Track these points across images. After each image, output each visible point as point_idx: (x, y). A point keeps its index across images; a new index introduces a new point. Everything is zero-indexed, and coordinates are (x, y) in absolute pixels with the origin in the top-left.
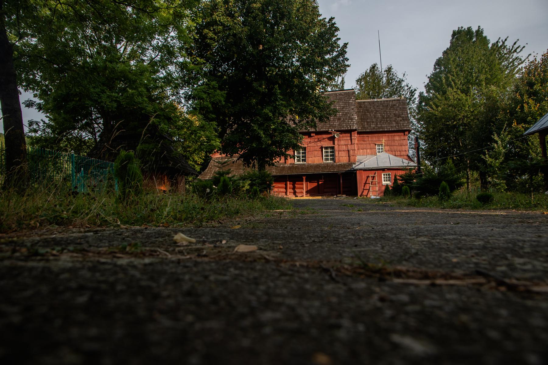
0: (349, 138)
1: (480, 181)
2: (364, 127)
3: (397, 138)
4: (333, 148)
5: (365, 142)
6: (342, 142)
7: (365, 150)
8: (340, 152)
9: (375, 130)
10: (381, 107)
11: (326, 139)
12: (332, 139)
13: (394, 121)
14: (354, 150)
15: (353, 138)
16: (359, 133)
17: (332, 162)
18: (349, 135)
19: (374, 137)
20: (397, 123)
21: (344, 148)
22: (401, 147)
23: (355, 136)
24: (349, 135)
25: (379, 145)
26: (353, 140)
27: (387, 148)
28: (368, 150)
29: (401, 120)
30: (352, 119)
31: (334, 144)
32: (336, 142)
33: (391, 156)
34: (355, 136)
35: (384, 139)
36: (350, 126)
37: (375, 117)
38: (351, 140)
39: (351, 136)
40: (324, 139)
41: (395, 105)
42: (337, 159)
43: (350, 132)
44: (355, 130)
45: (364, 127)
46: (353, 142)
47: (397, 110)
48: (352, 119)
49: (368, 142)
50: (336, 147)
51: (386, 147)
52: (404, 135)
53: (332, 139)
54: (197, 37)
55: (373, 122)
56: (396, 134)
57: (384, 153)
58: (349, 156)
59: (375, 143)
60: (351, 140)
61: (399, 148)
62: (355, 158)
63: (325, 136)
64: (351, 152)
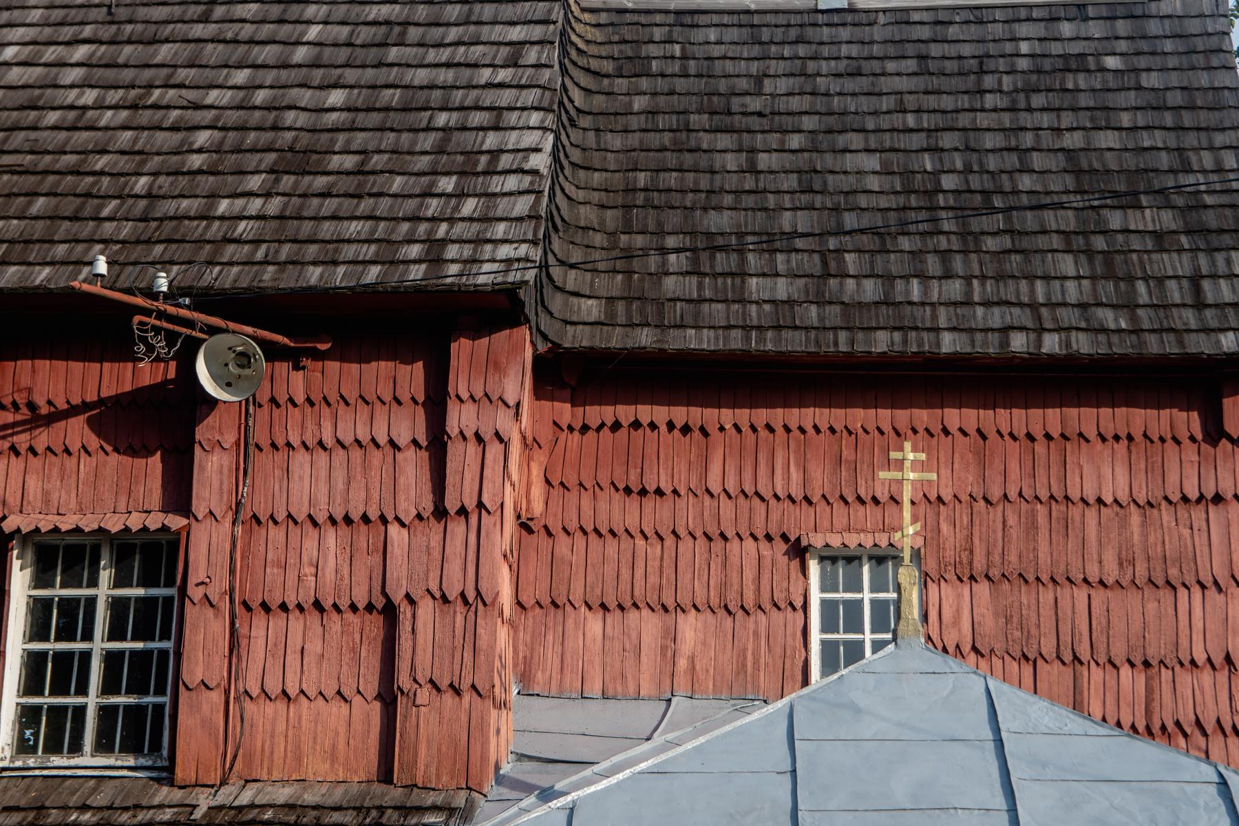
0: (408, 425)
1: (328, 363)
2: (641, 301)
3: (1105, 474)
4: (155, 556)
5: (657, 514)
6: (308, 483)
7: (649, 626)
8: (260, 632)
9: (795, 343)
10: (900, 78)
11: (77, 430)
12: (161, 425)
13: (1071, 242)
14: (476, 601)
15: (460, 418)
16: (560, 374)
17: (120, 762)
18: (412, 377)
19: (790, 450)
20: (1110, 267)
21: (329, 562)
22: (1156, 605)
23: (497, 385)
24: (412, 377)
25: (841, 560)
26: (461, 458)
27: (963, 606)
28: (690, 628)
29: (1161, 239)
30: (474, 168)
31: (178, 494)
32: (212, 472)
33: (1031, 715)
34: (497, 385)
35: (911, 465)
36: (435, 247)
37: (809, 182)
38: (437, 446)
39: (436, 403)
40: (38, 419)
41: (1075, 64)
42: (197, 723)
43: (419, 326)
44: (497, 310)
45: (641, 301)
46: (460, 491)
47: (1102, 117)
48: (474, 168)
49: (689, 513)
50: (208, 548)
51: (950, 596)
52: (1215, 432)
53: (161, 425)
54: (883, 474)
55: (772, 242)
56: (1086, 418)
57: (914, 653)
58: (388, 697)
59: (798, 522)
60: (437, 446)
61: (1133, 617)
62: (476, 731)
63: (55, 380)
64: (425, 631)
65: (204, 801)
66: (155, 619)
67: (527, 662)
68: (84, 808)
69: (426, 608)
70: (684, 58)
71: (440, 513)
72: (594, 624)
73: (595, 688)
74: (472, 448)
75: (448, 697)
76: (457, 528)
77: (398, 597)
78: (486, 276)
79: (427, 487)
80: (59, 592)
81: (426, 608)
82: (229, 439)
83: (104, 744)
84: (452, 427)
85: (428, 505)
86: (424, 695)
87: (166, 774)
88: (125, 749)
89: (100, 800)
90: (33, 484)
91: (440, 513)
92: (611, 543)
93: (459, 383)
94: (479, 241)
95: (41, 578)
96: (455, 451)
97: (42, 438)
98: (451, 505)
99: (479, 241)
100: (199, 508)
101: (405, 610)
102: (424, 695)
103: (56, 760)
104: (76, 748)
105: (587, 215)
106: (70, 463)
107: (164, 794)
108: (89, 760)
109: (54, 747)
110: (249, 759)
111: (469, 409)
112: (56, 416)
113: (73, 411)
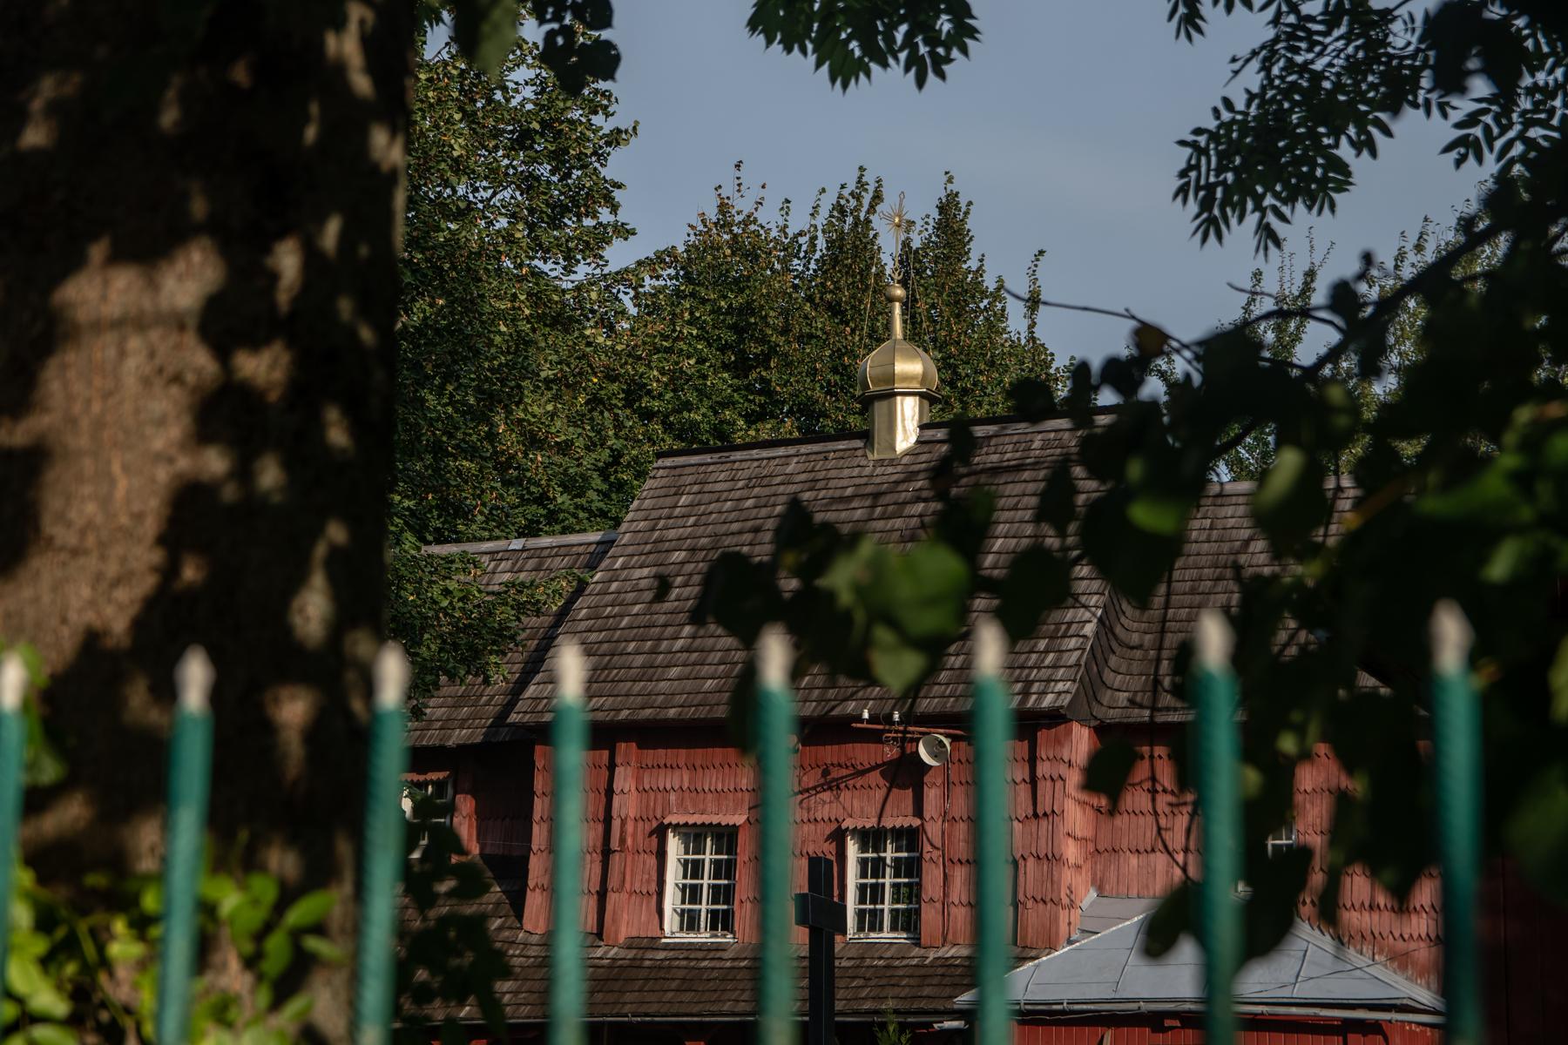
4: (909, 838)
11: (875, 777)
15: (1043, 769)
17: (901, 937)
26: (1044, 788)
31: (918, 811)
32: (932, 796)
46: (1044, 805)
62: (1054, 920)
65: (932, 955)
66: (910, 868)
67: (1102, 880)
68: (881, 958)
69: (1031, 862)
70: (1211, 528)
71: (1036, 815)
72: (1134, 860)
73: (1134, 893)
74: (1049, 783)
75: (1041, 905)
76: (1044, 823)
77: (1018, 856)
78: (1048, 701)
79: (1030, 803)
80: (870, 855)
81: (1031, 862)
82: (939, 781)
83: (894, 928)
84: (1039, 774)
85: (1030, 812)
86: (1030, 904)
87: (917, 942)
88: (903, 929)
89: (888, 954)
90: (856, 803)
91: (1036, 815)
92: (1141, 819)
93: (1042, 752)
94: (1049, 681)
95: (863, 849)
96: (1040, 785)
97: (859, 782)
98: (1040, 812)
99: (1049, 681)
100: (927, 816)
101: (1021, 862)
102: (1030, 904)
103: (873, 935)
104: (881, 930)
105: (1135, 638)
106: (871, 793)
107: (916, 951)
108: (886, 935)
109: (872, 929)
110: (954, 934)
111: (1047, 763)
112: (863, 773)
113: (872, 769)
